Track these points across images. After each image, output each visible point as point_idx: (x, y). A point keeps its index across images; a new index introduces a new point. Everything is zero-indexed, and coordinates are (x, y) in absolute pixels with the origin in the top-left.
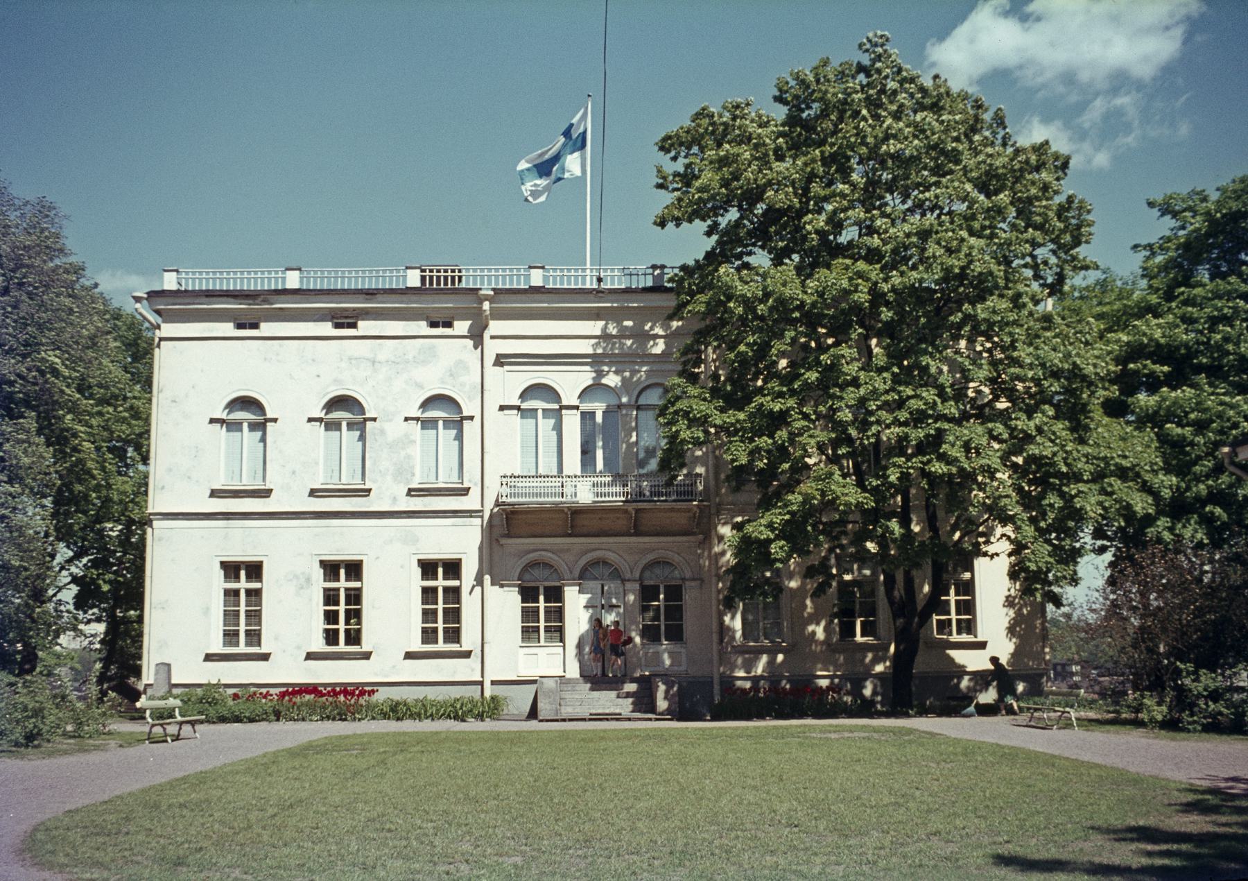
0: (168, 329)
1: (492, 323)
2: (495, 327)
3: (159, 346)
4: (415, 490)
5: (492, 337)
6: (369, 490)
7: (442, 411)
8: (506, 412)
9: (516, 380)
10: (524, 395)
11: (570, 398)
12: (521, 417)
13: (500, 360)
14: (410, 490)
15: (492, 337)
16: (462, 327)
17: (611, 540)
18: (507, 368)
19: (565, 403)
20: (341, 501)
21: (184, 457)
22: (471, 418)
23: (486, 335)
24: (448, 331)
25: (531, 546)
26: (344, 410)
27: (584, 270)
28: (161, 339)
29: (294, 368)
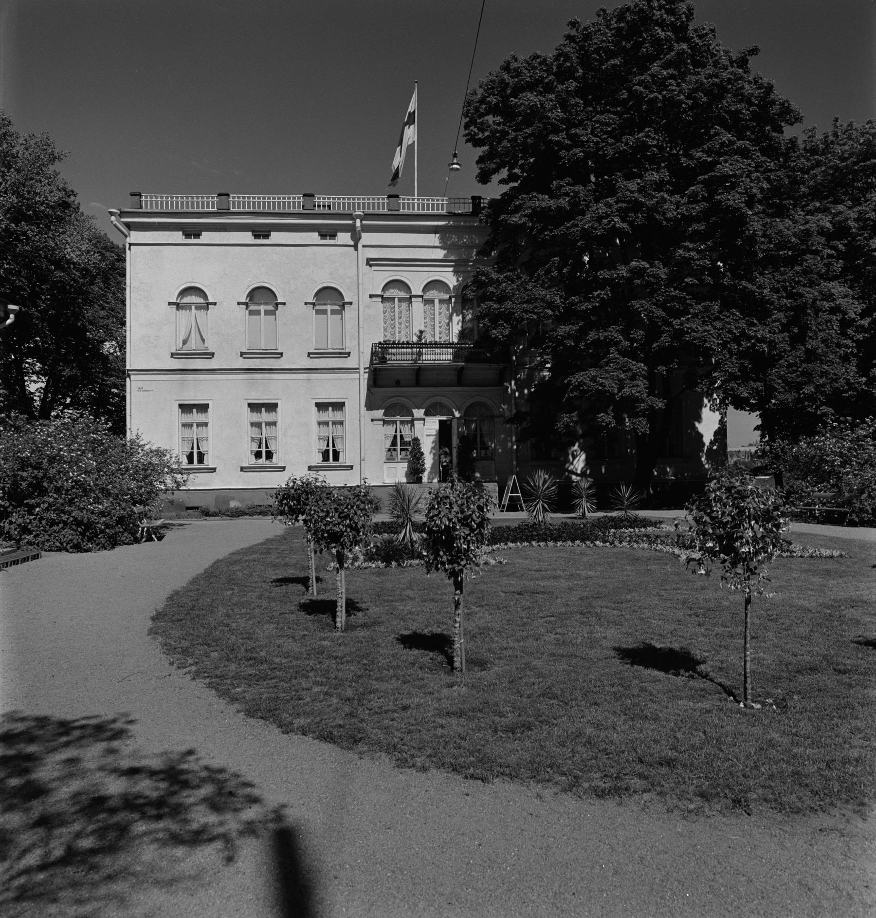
0: (135, 236)
1: (363, 235)
2: (367, 238)
3: (130, 249)
4: (246, 468)
5: (364, 246)
6: (281, 354)
7: (329, 297)
8: (374, 299)
9: (379, 278)
10: (386, 287)
11: (417, 290)
12: (390, 282)
13: (370, 262)
14: (309, 354)
15: (364, 246)
16: (344, 238)
17: (446, 389)
18: (374, 268)
19: (413, 293)
20: (261, 361)
21: (148, 330)
22: (351, 303)
23: (360, 246)
24: (332, 242)
25: (393, 383)
26: (261, 297)
27: (413, 200)
28: (130, 245)
29: (225, 265)
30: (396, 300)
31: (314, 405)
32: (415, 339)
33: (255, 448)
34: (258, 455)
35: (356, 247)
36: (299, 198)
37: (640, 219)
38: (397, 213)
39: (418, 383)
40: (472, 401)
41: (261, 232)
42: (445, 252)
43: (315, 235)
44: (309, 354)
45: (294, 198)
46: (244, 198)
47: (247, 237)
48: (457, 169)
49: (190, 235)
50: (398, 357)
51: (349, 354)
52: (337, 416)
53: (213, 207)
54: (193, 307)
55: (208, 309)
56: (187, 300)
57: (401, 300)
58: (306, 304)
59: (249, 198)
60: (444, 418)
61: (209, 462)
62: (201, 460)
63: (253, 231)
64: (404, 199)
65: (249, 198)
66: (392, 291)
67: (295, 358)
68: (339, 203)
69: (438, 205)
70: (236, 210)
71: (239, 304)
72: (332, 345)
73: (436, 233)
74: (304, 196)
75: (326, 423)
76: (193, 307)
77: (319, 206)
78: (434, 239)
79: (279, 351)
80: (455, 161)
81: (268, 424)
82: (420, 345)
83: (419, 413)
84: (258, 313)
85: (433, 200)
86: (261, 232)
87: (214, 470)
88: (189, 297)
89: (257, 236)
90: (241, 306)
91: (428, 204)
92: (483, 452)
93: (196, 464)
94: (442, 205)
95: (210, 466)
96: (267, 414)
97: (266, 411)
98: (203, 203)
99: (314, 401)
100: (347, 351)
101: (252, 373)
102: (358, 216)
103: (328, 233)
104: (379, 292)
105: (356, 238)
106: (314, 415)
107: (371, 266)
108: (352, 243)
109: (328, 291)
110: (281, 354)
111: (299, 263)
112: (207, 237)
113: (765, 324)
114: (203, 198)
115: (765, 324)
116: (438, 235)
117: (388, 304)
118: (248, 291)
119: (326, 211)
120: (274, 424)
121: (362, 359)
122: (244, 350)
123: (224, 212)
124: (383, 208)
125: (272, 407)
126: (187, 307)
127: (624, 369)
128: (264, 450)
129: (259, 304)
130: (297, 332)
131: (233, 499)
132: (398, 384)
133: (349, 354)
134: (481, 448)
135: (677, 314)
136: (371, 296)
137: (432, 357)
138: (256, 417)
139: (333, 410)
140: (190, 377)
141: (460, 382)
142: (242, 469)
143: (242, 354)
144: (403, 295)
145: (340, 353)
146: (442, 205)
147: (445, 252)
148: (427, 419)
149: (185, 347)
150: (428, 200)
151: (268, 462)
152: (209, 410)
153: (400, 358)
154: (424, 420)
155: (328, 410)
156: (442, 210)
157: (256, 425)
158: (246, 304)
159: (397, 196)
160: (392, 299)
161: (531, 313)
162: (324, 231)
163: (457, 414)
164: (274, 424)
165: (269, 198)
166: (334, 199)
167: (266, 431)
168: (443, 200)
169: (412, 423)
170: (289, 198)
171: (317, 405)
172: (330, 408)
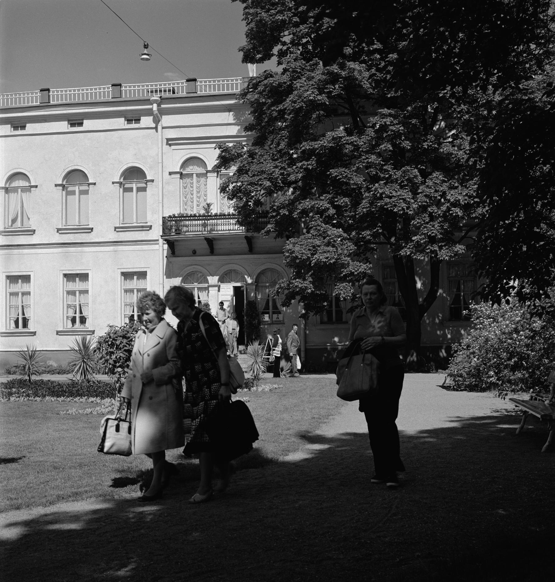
2: (166, 120)
5: (163, 128)
6: (92, 229)
8: (173, 176)
9: (176, 158)
13: (170, 142)
14: (116, 228)
15: (163, 128)
18: (173, 147)
23: (159, 128)
26: (75, 178)
30: (195, 175)
31: (119, 275)
32: (202, 212)
33: (71, 314)
34: (74, 320)
35: (156, 128)
36: (182, 83)
37: (336, 89)
38: (195, 95)
39: (212, 252)
40: (263, 268)
41: (76, 121)
42: (239, 127)
43: (122, 120)
44: (116, 228)
45: (104, 88)
46: (62, 91)
47: (63, 126)
48: (147, 59)
49: (18, 127)
50: (191, 229)
51: (150, 227)
52: (25, 288)
53: (36, 102)
54: (19, 190)
55: (30, 191)
56: (16, 184)
57: (198, 175)
58: (113, 183)
59: (66, 91)
60: (238, 284)
61: (31, 327)
62: (25, 325)
63: (69, 121)
64: (201, 82)
65: (66, 91)
66: (191, 167)
67: (104, 232)
68: (87, 94)
69: (232, 84)
70: (56, 102)
71: (56, 185)
72: (74, 222)
73: (229, 111)
74: (113, 85)
75: (16, 294)
76: (19, 190)
77: (165, 91)
78: (229, 117)
79: (90, 226)
80: (146, 52)
81: (81, 292)
82: (207, 216)
83: (213, 280)
84: (131, 190)
85: (228, 81)
86: (76, 121)
87: (34, 334)
88: (17, 182)
89: (16, 128)
90: (58, 187)
91: (223, 85)
92: (275, 316)
93: (21, 329)
94: (237, 84)
95: (31, 331)
96: (81, 283)
97: (80, 280)
98: (28, 98)
99: (120, 271)
100: (149, 224)
101: (66, 247)
102: (155, 101)
103: (133, 118)
104: (178, 170)
105: (157, 121)
106: (118, 282)
107: (170, 145)
108: (154, 125)
109: (81, 173)
110: (92, 229)
111: (109, 147)
112: (31, 128)
113: (466, 186)
114: (12, 95)
115: (466, 186)
116: (231, 113)
117: (188, 180)
118: (64, 174)
119: (171, 95)
120: (86, 292)
121: (157, 232)
122: (60, 227)
123: (46, 105)
124: (183, 92)
125: (84, 277)
126: (15, 190)
127: (324, 235)
128: (78, 315)
129: (74, 185)
130: (104, 208)
131: (50, 359)
132: (194, 253)
133: (150, 227)
134: (274, 313)
135: (375, 179)
136: (170, 173)
137: (227, 227)
138: (71, 286)
139: (138, 279)
140: (16, 251)
141: (251, 250)
142: (58, 333)
143: (58, 230)
144: (201, 170)
145: (142, 227)
146: (237, 84)
147: (239, 127)
148: (223, 286)
149: (14, 226)
150: (223, 81)
151: (82, 326)
152: (148, 277)
153: (194, 229)
154: (219, 287)
155: (18, 282)
156: (237, 89)
157: (72, 293)
158: (63, 186)
159: (195, 80)
160: (190, 175)
161: (256, 185)
162: (130, 117)
163: (249, 281)
164: (86, 292)
165: (83, 90)
166: (139, 86)
167: (77, 300)
168: (237, 80)
169: (207, 289)
170: (100, 89)
171: (123, 274)
172: (135, 277)
